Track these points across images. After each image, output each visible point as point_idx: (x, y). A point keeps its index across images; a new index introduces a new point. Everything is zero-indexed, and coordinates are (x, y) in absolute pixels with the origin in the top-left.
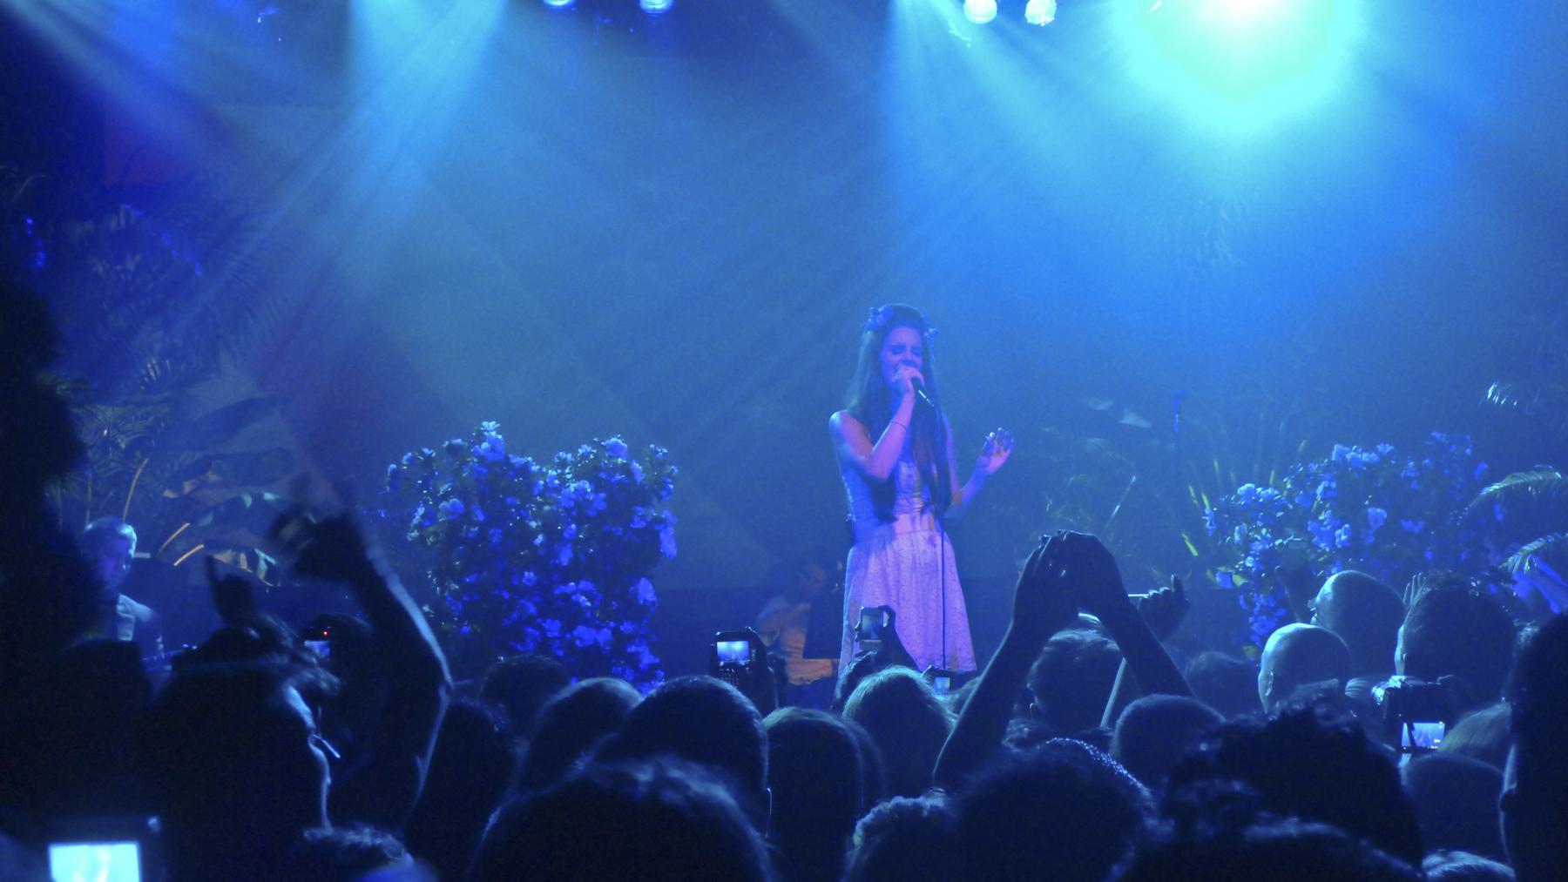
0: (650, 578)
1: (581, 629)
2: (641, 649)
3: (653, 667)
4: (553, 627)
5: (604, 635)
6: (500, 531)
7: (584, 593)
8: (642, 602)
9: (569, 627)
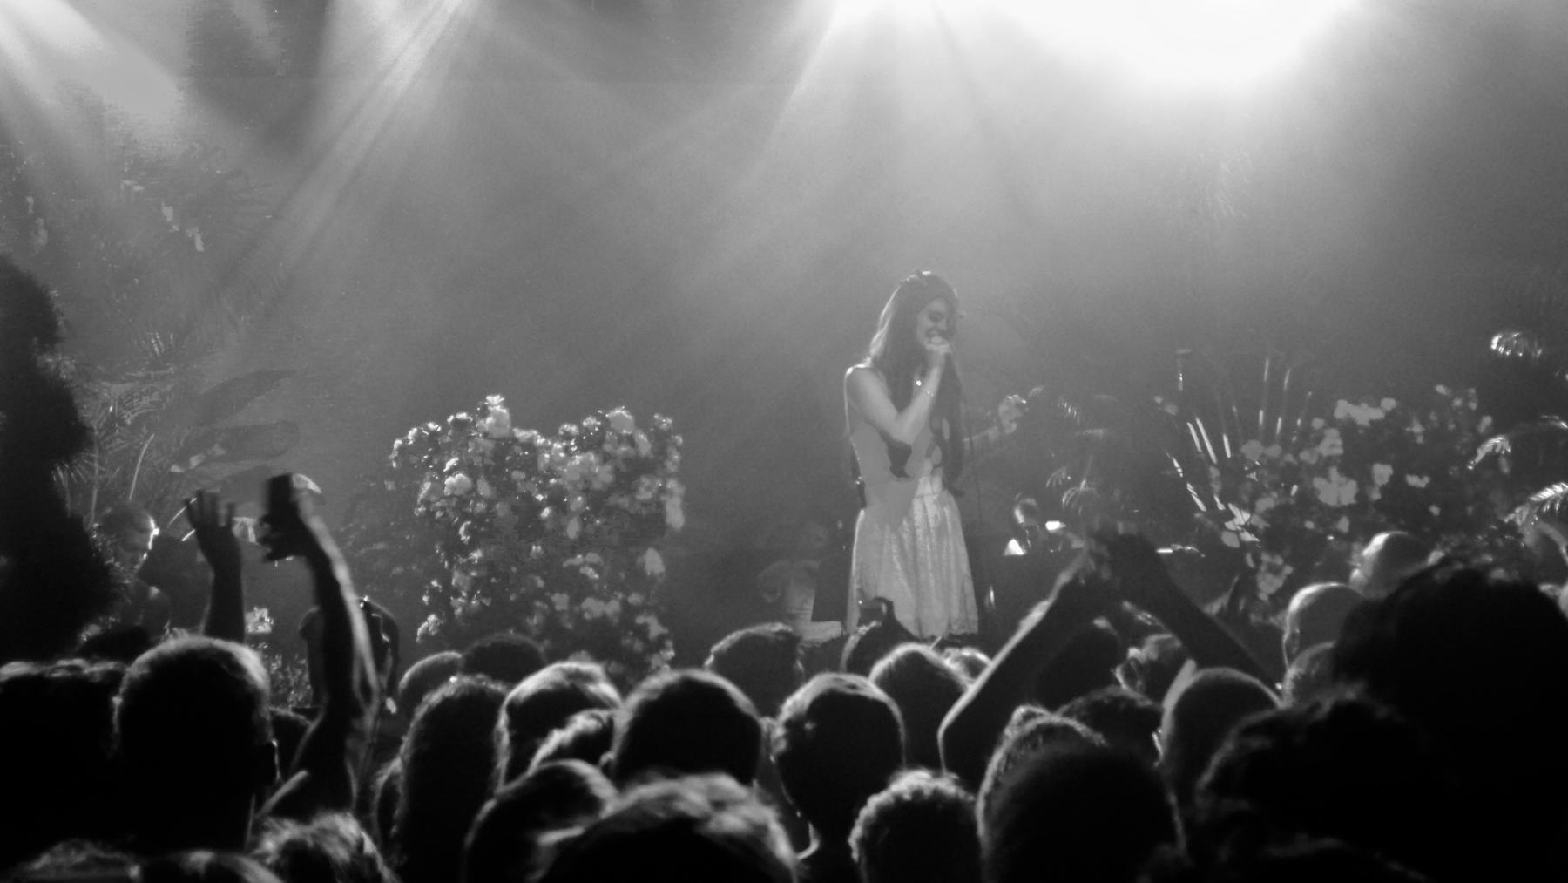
0: (658, 548)
4: (561, 601)
7: (593, 565)
9: (577, 599)
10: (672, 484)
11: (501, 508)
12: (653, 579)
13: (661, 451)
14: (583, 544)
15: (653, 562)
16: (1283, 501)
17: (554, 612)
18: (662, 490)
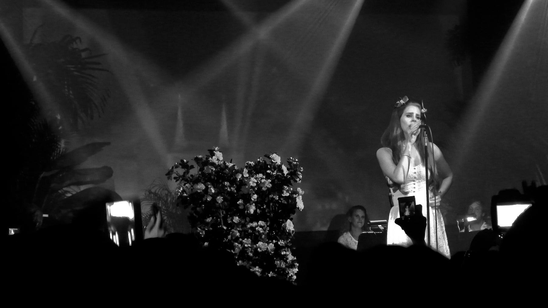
0: (291, 219)
1: (260, 243)
2: (288, 253)
3: (293, 261)
4: (247, 242)
5: (271, 246)
6: (222, 198)
7: (261, 227)
8: (288, 231)
9: (255, 241)
10: (299, 189)
11: (220, 199)
12: (289, 234)
13: (293, 174)
14: (255, 218)
15: (290, 226)
16: (185, 229)
17: (244, 248)
18: (295, 192)
